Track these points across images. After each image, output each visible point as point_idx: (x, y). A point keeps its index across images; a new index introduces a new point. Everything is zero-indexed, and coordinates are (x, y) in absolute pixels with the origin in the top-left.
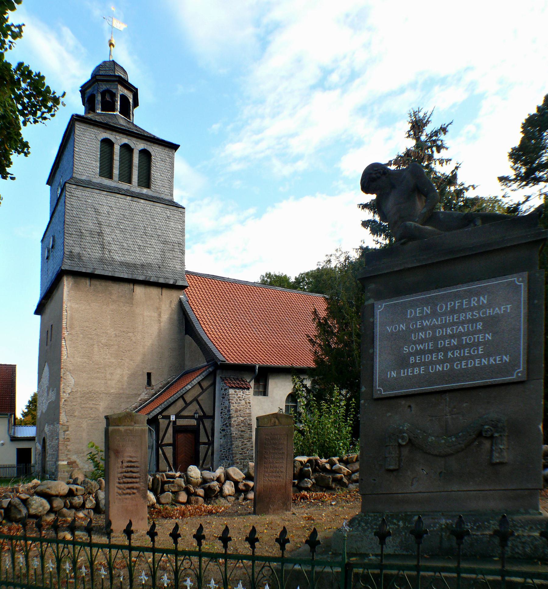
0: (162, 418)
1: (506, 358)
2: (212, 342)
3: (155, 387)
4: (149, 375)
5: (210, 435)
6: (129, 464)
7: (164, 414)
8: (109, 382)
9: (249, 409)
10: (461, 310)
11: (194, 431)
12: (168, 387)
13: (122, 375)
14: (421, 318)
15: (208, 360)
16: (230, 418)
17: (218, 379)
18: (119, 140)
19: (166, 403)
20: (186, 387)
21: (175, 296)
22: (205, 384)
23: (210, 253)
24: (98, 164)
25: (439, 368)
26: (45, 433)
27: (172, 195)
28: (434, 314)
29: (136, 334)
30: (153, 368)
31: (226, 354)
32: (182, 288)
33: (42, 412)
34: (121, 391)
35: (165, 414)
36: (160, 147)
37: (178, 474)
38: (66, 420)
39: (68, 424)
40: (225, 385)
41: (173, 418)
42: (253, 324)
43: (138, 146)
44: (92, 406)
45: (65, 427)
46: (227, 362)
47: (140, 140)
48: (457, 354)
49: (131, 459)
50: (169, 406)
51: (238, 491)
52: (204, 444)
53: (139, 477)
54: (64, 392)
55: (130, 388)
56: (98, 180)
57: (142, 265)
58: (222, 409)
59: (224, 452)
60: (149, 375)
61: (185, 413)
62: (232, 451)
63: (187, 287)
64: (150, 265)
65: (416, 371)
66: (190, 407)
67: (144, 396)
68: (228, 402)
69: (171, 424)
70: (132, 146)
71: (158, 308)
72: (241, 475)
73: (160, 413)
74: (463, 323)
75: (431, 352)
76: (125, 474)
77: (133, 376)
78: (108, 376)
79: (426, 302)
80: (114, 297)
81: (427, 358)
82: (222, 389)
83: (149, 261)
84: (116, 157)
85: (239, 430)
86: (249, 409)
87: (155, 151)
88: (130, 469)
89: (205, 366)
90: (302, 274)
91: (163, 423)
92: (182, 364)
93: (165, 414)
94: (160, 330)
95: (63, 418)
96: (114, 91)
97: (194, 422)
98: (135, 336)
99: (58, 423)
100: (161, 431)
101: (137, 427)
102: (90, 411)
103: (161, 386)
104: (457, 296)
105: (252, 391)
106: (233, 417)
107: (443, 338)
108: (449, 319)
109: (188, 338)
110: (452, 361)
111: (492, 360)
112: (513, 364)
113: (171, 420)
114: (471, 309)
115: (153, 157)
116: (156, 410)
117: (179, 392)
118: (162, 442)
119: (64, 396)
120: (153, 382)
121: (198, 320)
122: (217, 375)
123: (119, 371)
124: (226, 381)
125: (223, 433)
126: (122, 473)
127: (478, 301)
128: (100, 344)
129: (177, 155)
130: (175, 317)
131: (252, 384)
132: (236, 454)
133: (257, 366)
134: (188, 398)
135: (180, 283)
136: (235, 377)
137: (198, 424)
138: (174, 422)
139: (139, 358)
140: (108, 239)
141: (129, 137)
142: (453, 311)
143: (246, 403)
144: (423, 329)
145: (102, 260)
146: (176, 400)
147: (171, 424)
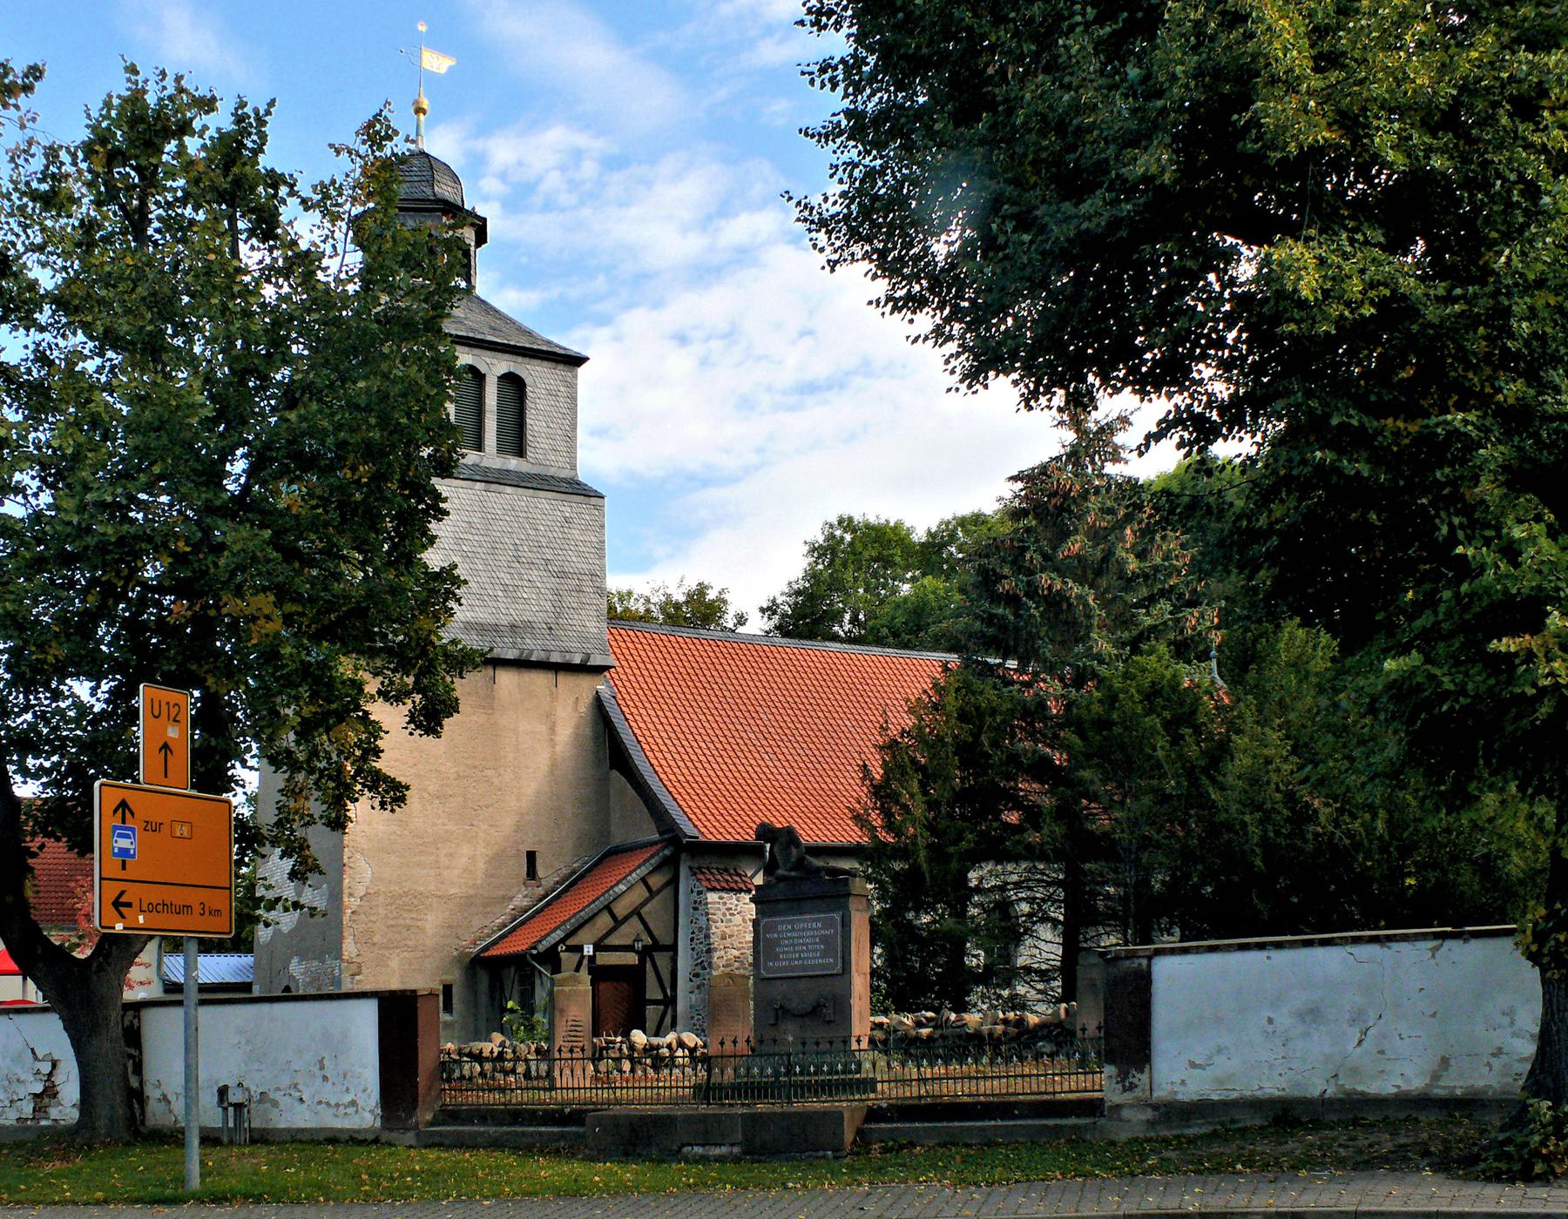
4: (531, 856)
5: (667, 984)
7: (568, 943)
8: (446, 873)
11: (633, 977)
12: (574, 881)
13: (473, 858)
16: (709, 951)
17: (684, 872)
21: (586, 687)
22: (656, 881)
23: (682, 339)
26: (292, 977)
27: (574, 467)
29: (501, 770)
30: (540, 842)
32: (600, 670)
34: (471, 892)
35: (571, 942)
36: (545, 363)
37: (619, 1039)
38: (354, 952)
39: (359, 960)
41: (588, 950)
43: (495, 367)
44: (408, 922)
45: (354, 968)
46: (702, 839)
47: (499, 355)
50: (581, 926)
54: (351, 895)
57: (513, 627)
60: (531, 856)
61: (614, 940)
64: (529, 626)
66: (624, 928)
67: (520, 901)
69: (585, 962)
70: (483, 369)
71: (548, 715)
73: (562, 941)
77: (497, 859)
78: (444, 861)
87: (535, 374)
89: (655, 843)
90: (948, 523)
92: (603, 831)
93: (571, 942)
94: (553, 766)
95: (349, 948)
97: (631, 959)
99: (339, 956)
101: (581, 988)
102: (406, 934)
104: (804, 921)
106: (716, 950)
112: (836, 963)
115: (529, 389)
119: (350, 903)
120: (541, 872)
123: (466, 850)
129: (582, 370)
130: (588, 731)
134: (621, 909)
135: (596, 660)
138: (592, 959)
139: (508, 823)
141: (477, 351)
146: (596, 915)
147: (585, 962)
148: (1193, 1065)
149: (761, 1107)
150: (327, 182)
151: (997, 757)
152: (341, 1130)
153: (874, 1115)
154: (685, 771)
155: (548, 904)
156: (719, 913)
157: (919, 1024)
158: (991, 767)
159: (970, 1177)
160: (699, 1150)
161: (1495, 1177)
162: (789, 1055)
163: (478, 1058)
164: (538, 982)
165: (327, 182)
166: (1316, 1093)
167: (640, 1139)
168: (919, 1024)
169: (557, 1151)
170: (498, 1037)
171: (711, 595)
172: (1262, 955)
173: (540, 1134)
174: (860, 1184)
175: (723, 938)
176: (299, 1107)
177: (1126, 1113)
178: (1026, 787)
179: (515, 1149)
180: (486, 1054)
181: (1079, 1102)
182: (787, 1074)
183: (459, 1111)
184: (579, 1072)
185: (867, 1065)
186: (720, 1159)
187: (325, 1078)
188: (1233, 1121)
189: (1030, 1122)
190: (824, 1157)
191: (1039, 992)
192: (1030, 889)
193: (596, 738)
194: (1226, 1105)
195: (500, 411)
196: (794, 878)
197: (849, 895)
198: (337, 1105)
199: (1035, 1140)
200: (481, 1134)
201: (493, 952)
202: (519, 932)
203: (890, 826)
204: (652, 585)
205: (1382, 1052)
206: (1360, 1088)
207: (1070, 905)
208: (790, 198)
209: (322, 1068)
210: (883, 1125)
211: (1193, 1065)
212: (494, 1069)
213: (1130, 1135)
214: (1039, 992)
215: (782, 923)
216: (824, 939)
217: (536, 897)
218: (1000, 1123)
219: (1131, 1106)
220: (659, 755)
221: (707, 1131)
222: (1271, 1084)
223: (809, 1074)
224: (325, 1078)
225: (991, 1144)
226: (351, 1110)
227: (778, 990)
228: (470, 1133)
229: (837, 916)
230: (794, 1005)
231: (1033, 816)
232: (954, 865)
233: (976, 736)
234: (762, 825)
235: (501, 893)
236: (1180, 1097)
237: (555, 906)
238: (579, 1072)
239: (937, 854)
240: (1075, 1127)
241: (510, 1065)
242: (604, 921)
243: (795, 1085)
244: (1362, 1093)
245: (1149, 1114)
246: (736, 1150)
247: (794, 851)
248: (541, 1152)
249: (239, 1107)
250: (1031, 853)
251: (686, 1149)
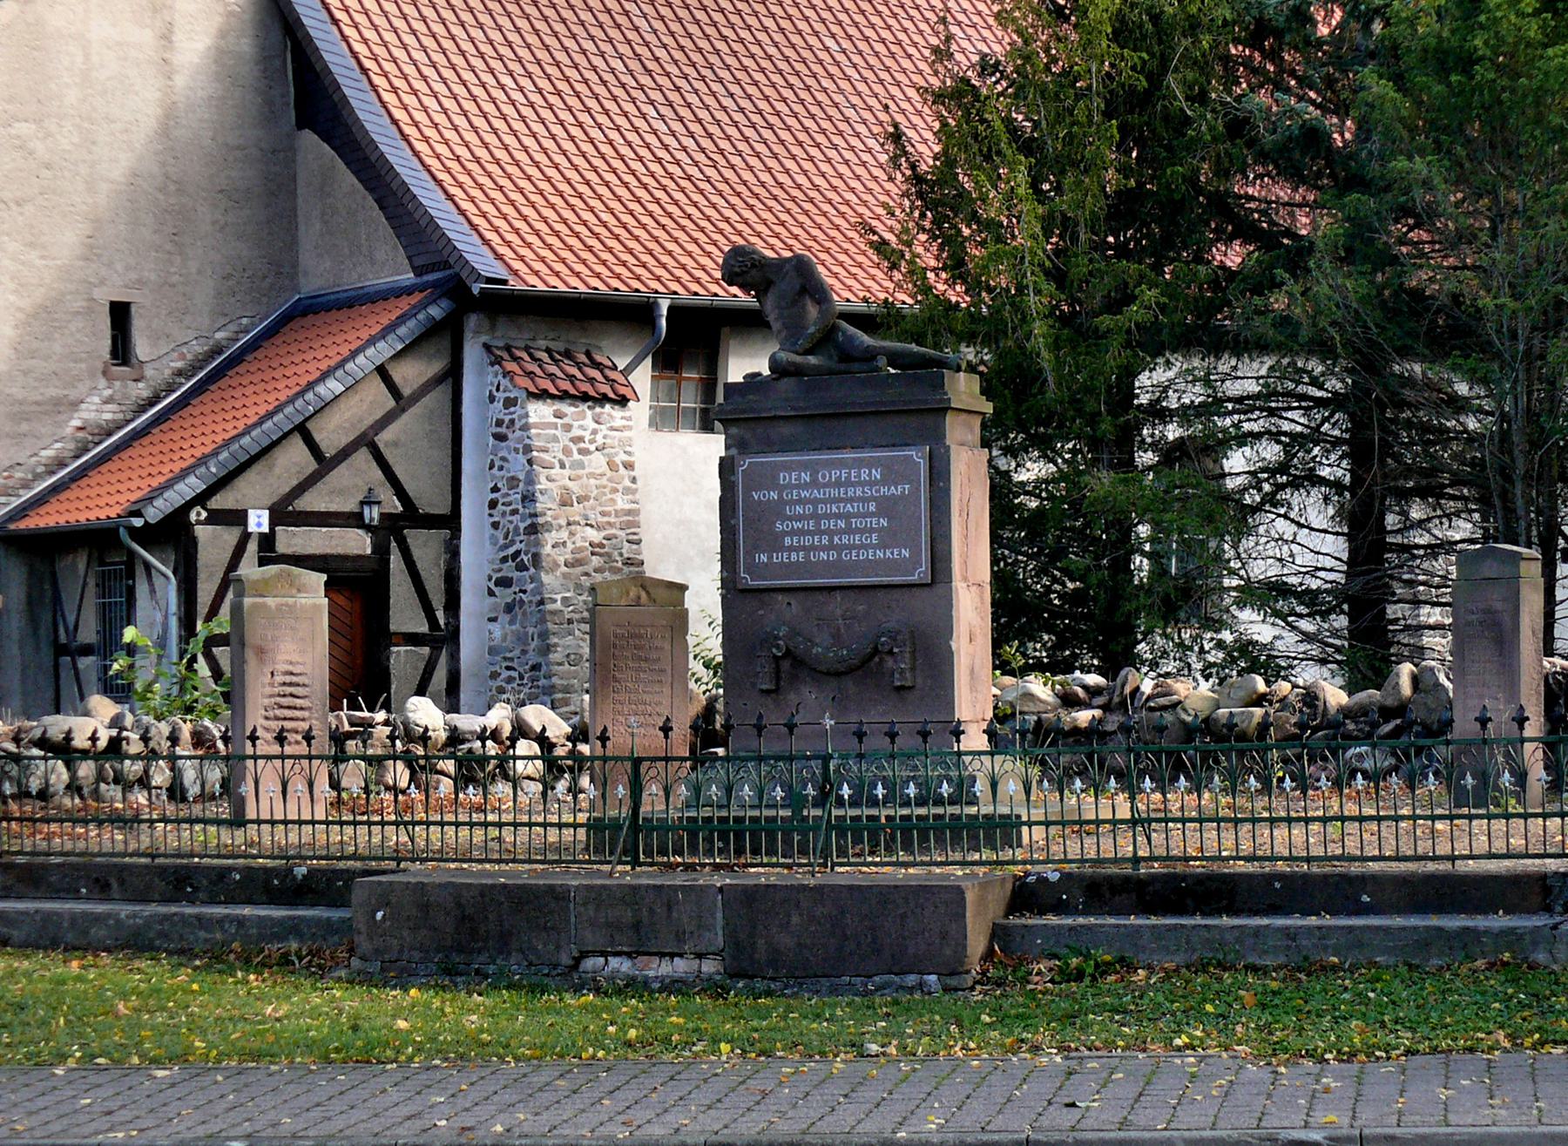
0: (208, 522)
1: (906, 553)
2: (439, 182)
3: (149, 372)
4: (120, 314)
5: (438, 601)
6: (288, 679)
7: (216, 502)
9: (627, 491)
10: (848, 483)
12: (218, 371)
14: (798, 487)
15: (419, 262)
16: (533, 529)
17: (472, 354)
19: (224, 455)
20: (321, 389)
22: (410, 374)
25: (823, 556)
28: (814, 483)
30: (141, 283)
31: (508, 244)
40: (505, 382)
41: (258, 521)
42: (645, 80)
46: (514, 284)
48: (845, 541)
49: (291, 668)
51: (553, 768)
52: (413, 639)
53: (309, 709)
55: (25, 373)
58: (495, 489)
59: (510, 680)
60: (120, 314)
61: (312, 501)
62: (548, 677)
65: (794, 556)
66: (341, 476)
67: (96, 408)
68: (522, 459)
69: (252, 547)
72: (559, 728)
73: (201, 499)
74: (851, 500)
75: (809, 533)
76: (279, 699)
77: (43, 319)
79: (804, 466)
81: (807, 541)
82: (492, 399)
85: (578, 586)
86: (627, 491)
88: (289, 690)
89: (409, 291)
91: (213, 543)
97: (358, 543)
98: (49, 135)
100: (202, 576)
101: (304, 600)
103: (179, 364)
104: (841, 464)
105: (640, 410)
106: (548, 527)
107: (828, 516)
108: (834, 492)
109: (313, 148)
110: (840, 548)
111: (888, 554)
113: (252, 528)
114: (862, 484)
116: (180, 486)
117: (289, 410)
120: (142, 348)
121: (364, 71)
122: (468, 335)
124: (511, 366)
125: (505, 595)
126: (271, 696)
127: (870, 474)
130: (246, 45)
131: (643, 378)
132: (567, 690)
133: (664, 305)
134: (332, 433)
136: (559, 346)
137: (381, 551)
139: (67, 239)
142: (838, 484)
143: (612, 465)
144: (800, 501)
146: (274, 444)
147: (252, 547)
149: (761, 874)
151: (1206, 124)
153: (1026, 896)
154: (470, 137)
156: (556, 449)
157: (1069, 701)
158: (1192, 145)
159: (1294, 1041)
160: (621, 965)
162: (826, 759)
163: (63, 749)
164: (142, 589)
167: (479, 935)
168: (1069, 701)
169: (285, 961)
170: (103, 708)
173: (241, 922)
174: (1036, 1049)
175: (565, 503)
178: (1259, 189)
179: (184, 953)
180: (80, 741)
181: (1515, 881)
182: (821, 801)
183: (46, 867)
184: (298, 786)
185: (981, 787)
186: (673, 986)
189: (1398, 921)
191: (1308, 637)
192: (1272, 413)
193: (265, 59)
196: (817, 371)
197: (943, 410)
199: (1416, 955)
200: (97, 919)
201: (22, 525)
202: (94, 478)
203: (956, 267)
207: (1359, 452)
210: (1053, 920)
212: (101, 777)
214: (1308, 637)
215: (788, 467)
216: (887, 507)
218: (1328, 921)
220: (410, 100)
221: (641, 925)
223: (874, 802)
227: (784, 616)
228: (74, 918)
229: (918, 456)
230: (821, 648)
231: (1285, 255)
232: (1113, 357)
233: (1156, 79)
234: (737, 251)
235: (53, 392)
237: (175, 422)
238: (298, 786)
239: (1074, 330)
240: (1510, 938)
241: (138, 767)
242: (294, 460)
243: (840, 827)
246: (709, 967)
247: (812, 311)
248: (247, 962)
250: (1282, 339)
251: (591, 963)
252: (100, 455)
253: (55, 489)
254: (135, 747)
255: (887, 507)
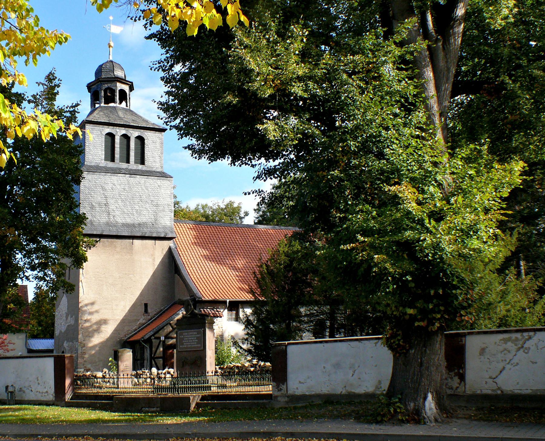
3: (150, 314)
4: (146, 305)
12: (161, 314)
18: (119, 132)
21: (166, 244)
24: (104, 152)
26: (64, 348)
33: (61, 332)
35: (157, 335)
37: (147, 371)
41: (162, 338)
43: (134, 134)
56: (103, 163)
60: (146, 305)
63: (174, 238)
67: (142, 321)
69: (161, 343)
73: (153, 335)
80: (118, 249)
83: (144, 220)
84: (117, 146)
87: (149, 136)
91: (155, 342)
93: (157, 335)
96: (114, 88)
99: (77, 341)
112: (201, 346)
115: (146, 141)
118: (154, 355)
120: (149, 310)
128: (108, 284)
130: (167, 261)
138: (164, 342)
140: (112, 207)
145: (108, 224)
147: (161, 343)
148: (300, 382)
150: (36, 94)
152: (43, 401)
155: (152, 322)
160: (147, 409)
161: (369, 422)
164: (145, 350)
165: (36, 94)
166: (339, 393)
171: (235, 205)
172: (321, 345)
176: (31, 393)
177: (279, 399)
187: (39, 384)
188: (312, 402)
190: (184, 412)
194: (311, 396)
195: (136, 149)
198: (42, 393)
201: (131, 339)
204: (213, 202)
205: (360, 379)
206: (353, 391)
208: (155, 102)
209: (38, 380)
211: (300, 382)
213: (280, 406)
215: (185, 332)
216: (198, 338)
217: (147, 320)
219: (281, 396)
222: (325, 390)
224: (39, 384)
225: (237, 408)
226: (46, 394)
235: (135, 318)
236: (296, 393)
241: (108, 380)
244: (354, 393)
245: (286, 399)
246: (158, 409)
249: (11, 392)
251: (143, 409)
252: (142, 327)
253: (136, 334)
254: (108, 376)
255: (198, 338)
